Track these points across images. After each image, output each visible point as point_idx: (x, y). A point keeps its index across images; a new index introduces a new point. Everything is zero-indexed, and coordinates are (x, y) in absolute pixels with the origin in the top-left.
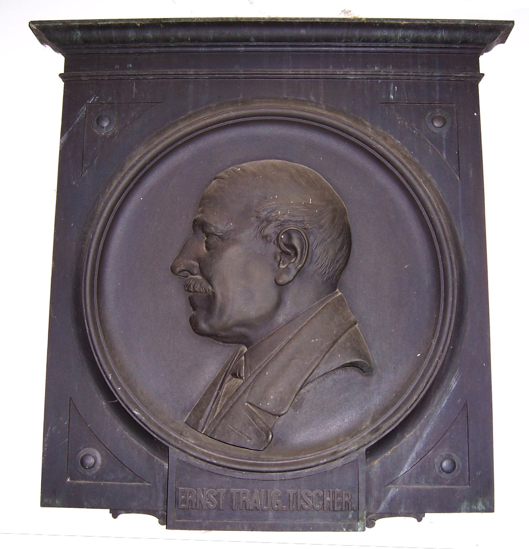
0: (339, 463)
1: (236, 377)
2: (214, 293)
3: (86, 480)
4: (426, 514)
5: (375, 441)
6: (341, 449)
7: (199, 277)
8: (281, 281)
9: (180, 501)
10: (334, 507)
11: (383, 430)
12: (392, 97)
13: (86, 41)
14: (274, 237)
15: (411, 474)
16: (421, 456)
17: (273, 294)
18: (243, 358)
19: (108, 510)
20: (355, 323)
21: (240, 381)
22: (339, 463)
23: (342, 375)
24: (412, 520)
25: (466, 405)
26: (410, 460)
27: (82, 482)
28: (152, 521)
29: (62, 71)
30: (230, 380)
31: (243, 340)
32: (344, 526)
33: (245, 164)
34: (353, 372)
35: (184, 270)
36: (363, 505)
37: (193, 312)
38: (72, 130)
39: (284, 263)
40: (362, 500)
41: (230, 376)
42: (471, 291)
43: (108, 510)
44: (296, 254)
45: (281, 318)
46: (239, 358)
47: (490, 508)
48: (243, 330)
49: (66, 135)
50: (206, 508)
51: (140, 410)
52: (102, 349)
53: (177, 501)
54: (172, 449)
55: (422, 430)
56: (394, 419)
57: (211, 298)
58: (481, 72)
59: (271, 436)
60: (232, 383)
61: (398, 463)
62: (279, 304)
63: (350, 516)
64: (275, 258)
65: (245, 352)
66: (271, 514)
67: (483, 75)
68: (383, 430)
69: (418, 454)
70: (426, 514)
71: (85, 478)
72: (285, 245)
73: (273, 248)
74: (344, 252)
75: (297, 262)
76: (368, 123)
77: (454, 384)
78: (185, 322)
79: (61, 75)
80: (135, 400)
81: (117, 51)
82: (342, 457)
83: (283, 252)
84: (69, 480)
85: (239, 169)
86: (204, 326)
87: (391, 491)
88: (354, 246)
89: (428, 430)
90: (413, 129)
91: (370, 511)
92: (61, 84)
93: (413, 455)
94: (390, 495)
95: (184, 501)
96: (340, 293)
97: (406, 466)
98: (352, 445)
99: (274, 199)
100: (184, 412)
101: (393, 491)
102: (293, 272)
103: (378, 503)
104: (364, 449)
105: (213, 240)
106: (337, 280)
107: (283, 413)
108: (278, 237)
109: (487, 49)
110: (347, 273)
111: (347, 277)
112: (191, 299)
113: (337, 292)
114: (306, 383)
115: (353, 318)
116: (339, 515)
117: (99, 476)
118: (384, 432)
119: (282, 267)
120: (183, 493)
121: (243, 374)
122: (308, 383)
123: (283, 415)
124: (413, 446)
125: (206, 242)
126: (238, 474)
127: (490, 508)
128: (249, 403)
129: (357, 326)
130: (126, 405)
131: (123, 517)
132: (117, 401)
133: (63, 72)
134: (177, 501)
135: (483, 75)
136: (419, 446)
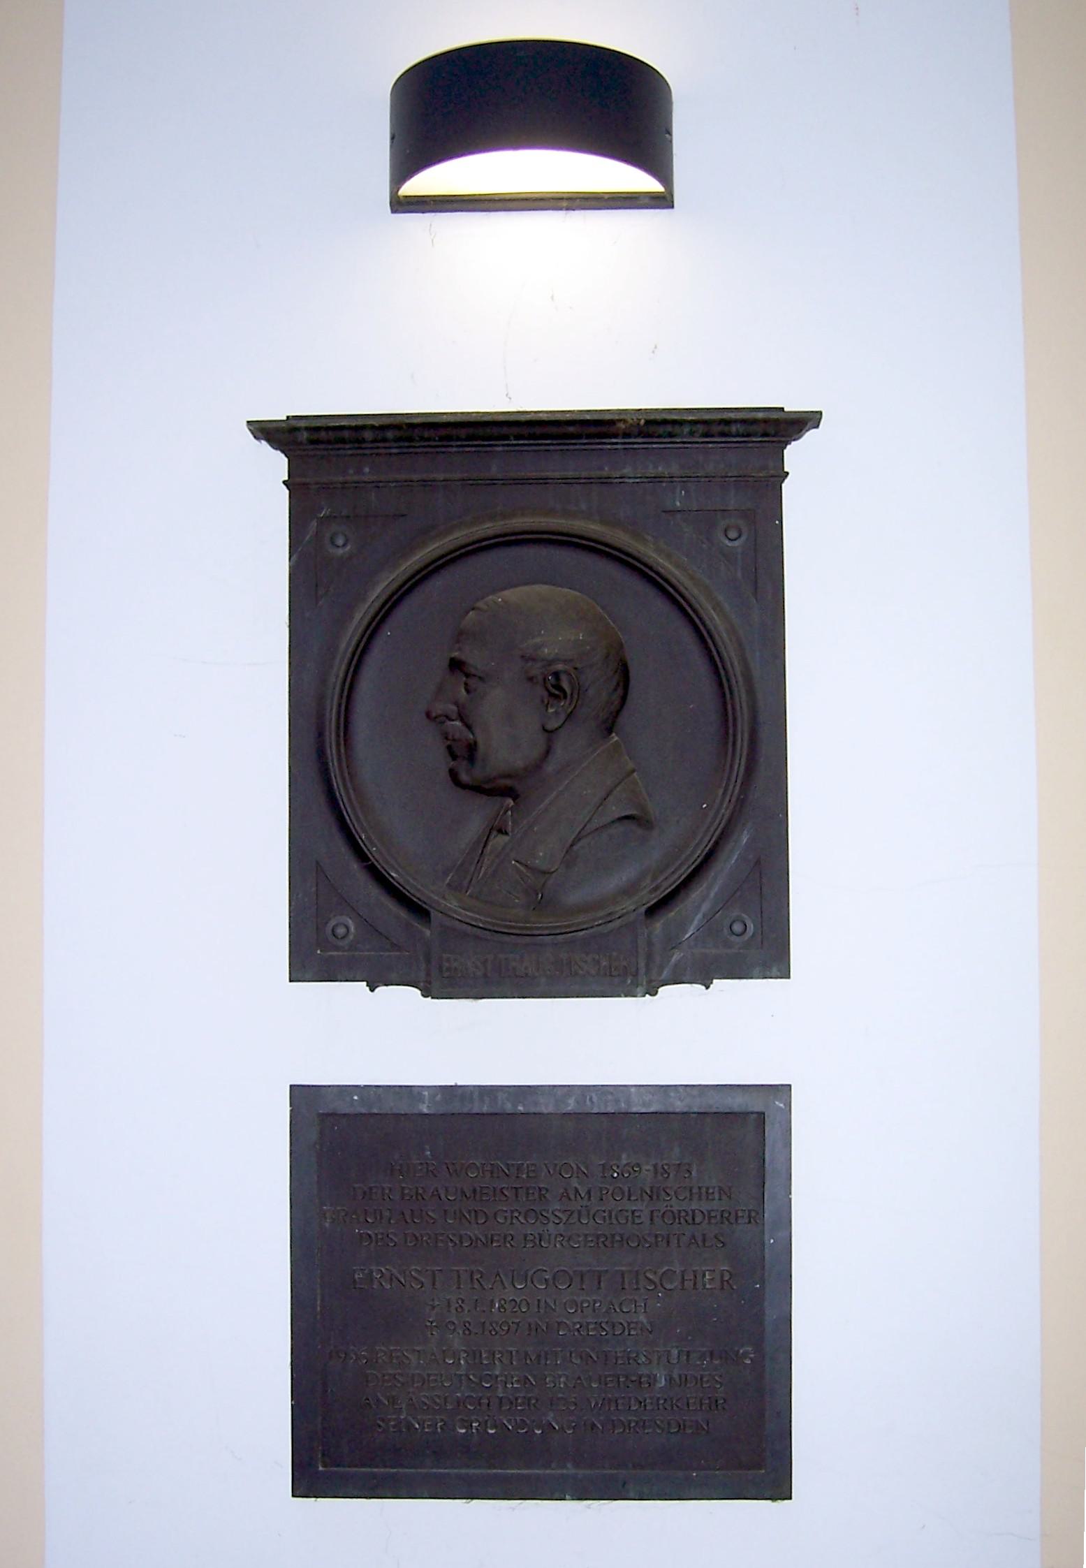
0: (617, 923)
1: (502, 833)
2: (475, 743)
3: (338, 951)
4: (715, 981)
5: (655, 901)
6: (617, 909)
7: (458, 723)
8: (550, 726)
9: (444, 969)
10: (611, 972)
11: (662, 889)
12: (678, 504)
13: (312, 442)
14: (540, 678)
15: (697, 937)
16: (709, 918)
17: (541, 739)
18: (510, 813)
19: (365, 983)
20: (633, 771)
21: (506, 838)
22: (617, 923)
23: (620, 829)
24: (699, 988)
25: (758, 862)
26: (696, 922)
27: (335, 953)
28: (416, 992)
29: (286, 478)
30: (495, 837)
31: (510, 792)
32: (623, 992)
33: (506, 593)
34: (631, 826)
35: (440, 716)
36: (642, 971)
37: (452, 763)
38: (302, 550)
39: (552, 706)
40: (642, 964)
41: (494, 833)
42: (764, 733)
43: (365, 983)
44: (565, 697)
45: (550, 768)
46: (505, 812)
47: (786, 975)
48: (508, 782)
49: (294, 557)
50: (472, 975)
51: (397, 872)
52: (353, 809)
53: (440, 968)
54: (433, 914)
55: (709, 888)
56: (676, 876)
57: (472, 748)
58: (786, 470)
59: (540, 895)
60: (499, 841)
61: (683, 927)
62: (548, 752)
63: (629, 982)
64: (543, 701)
65: (510, 806)
66: (543, 980)
67: (788, 473)
68: (662, 889)
69: (704, 916)
70: (715, 981)
71: (337, 948)
72: (553, 686)
73: (540, 691)
74: (620, 691)
75: (567, 703)
76: (649, 538)
77: (745, 839)
78: (444, 774)
79: (284, 482)
80: (393, 862)
81: (350, 452)
82: (619, 917)
83: (551, 695)
84: (319, 952)
85: (500, 600)
86: (464, 777)
87: (675, 957)
88: (632, 683)
89: (716, 889)
90: (703, 543)
91: (653, 978)
92: (286, 492)
93: (700, 916)
94: (674, 959)
95: (449, 969)
96: (616, 738)
97: (692, 928)
98: (628, 905)
99: (540, 635)
100: (446, 873)
101: (676, 956)
102: (563, 717)
103: (661, 968)
104: (643, 909)
105: (471, 682)
106: (614, 722)
107: (553, 870)
108: (544, 679)
109: (509, 776)
110: (625, 713)
111: (623, 719)
112: (449, 748)
113: (613, 738)
114: (578, 839)
115: (631, 765)
116: (616, 980)
117: (352, 947)
118: (664, 891)
119: (551, 710)
120: (448, 960)
121: (509, 829)
122: (579, 840)
123: (553, 872)
124: (699, 907)
125: (466, 684)
126: (506, 938)
127: (786, 975)
128: (517, 862)
129: (635, 774)
130: (383, 868)
131: (381, 990)
132: (370, 863)
133: (286, 478)
134: (440, 968)
135: (788, 473)
136: (705, 907)
